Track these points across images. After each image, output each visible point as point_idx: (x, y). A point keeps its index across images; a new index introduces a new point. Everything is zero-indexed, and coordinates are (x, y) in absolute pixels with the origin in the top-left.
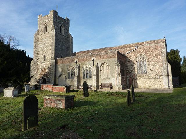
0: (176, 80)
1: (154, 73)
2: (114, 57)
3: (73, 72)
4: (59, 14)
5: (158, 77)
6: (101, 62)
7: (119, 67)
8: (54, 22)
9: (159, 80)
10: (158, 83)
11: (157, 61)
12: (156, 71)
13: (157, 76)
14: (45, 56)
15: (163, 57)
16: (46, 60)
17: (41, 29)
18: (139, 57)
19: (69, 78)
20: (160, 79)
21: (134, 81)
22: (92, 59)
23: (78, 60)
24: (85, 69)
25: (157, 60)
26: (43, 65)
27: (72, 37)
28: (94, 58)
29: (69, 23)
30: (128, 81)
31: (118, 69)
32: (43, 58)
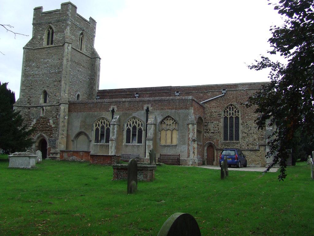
1: (251, 139)
3: (105, 129)
5: (257, 148)
6: (162, 115)
7: (196, 126)
9: (258, 153)
16: (48, 101)
18: (228, 110)
20: (260, 151)
21: (215, 154)
22: (145, 108)
23: (118, 107)
24: (99, 125)
27: (100, 59)
28: (149, 106)
29: (95, 28)
30: (205, 151)
31: (193, 130)
32: (42, 96)
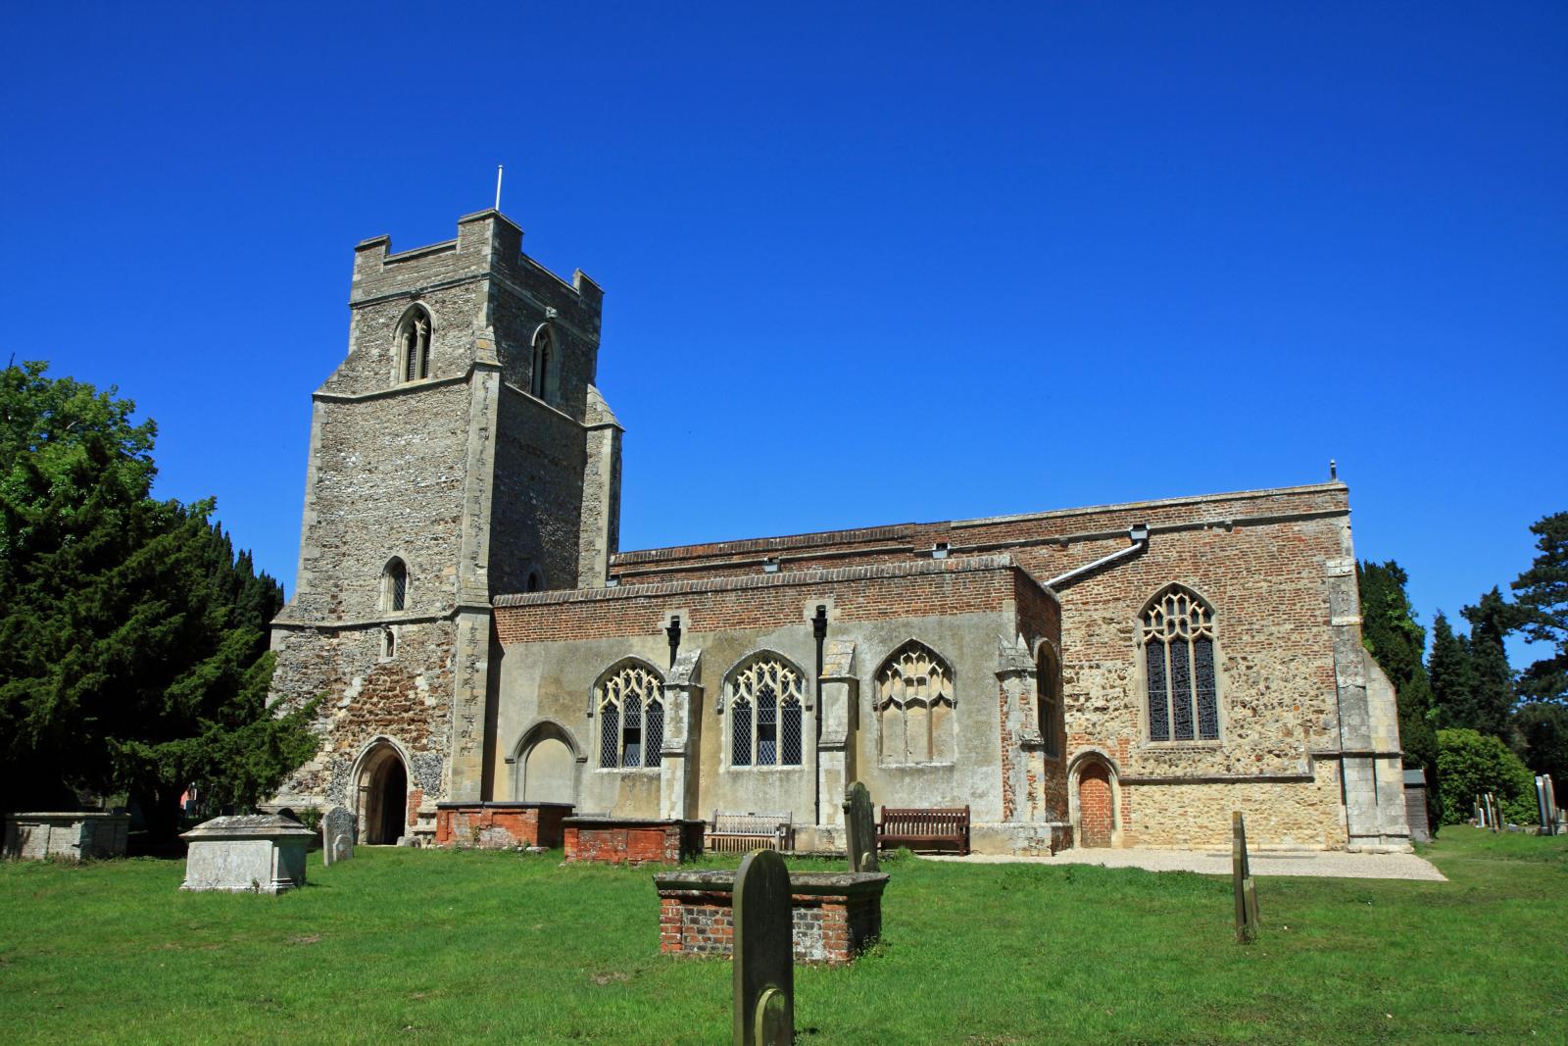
0: (1297, 526)
2: (989, 607)
3: (644, 708)
4: (526, 247)
5: (1301, 767)
8: (490, 301)
10: (1303, 814)
11: (1296, 644)
12: (1290, 719)
13: (1297, 757)
14: (397, 570)
15: (1336, 621)
16: (408, 602)
17: (375, 352)
19: (609, 760)
22: (810, 613)
25: (1295, 637)
26: (384, 643)
31: (1024, 698)
